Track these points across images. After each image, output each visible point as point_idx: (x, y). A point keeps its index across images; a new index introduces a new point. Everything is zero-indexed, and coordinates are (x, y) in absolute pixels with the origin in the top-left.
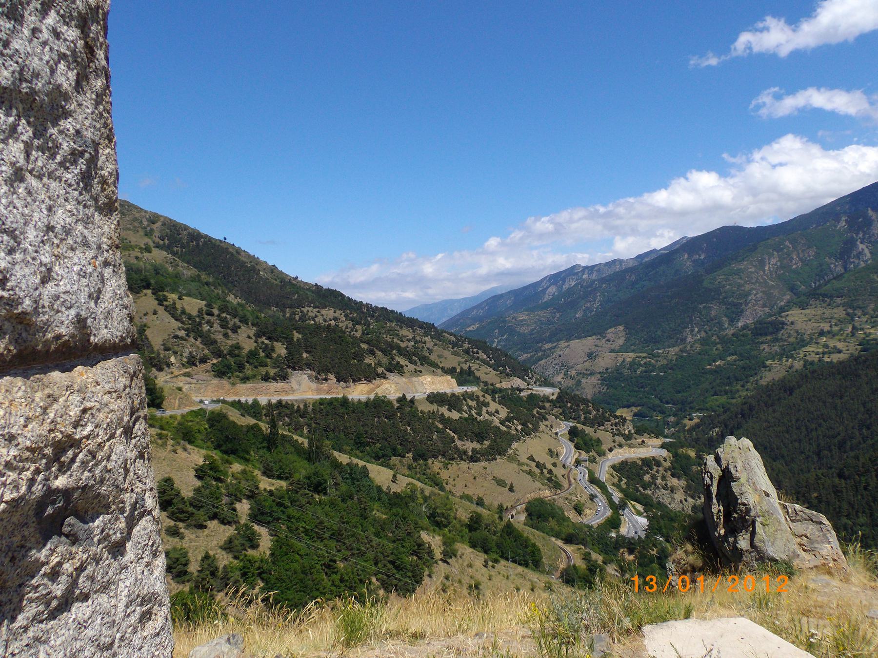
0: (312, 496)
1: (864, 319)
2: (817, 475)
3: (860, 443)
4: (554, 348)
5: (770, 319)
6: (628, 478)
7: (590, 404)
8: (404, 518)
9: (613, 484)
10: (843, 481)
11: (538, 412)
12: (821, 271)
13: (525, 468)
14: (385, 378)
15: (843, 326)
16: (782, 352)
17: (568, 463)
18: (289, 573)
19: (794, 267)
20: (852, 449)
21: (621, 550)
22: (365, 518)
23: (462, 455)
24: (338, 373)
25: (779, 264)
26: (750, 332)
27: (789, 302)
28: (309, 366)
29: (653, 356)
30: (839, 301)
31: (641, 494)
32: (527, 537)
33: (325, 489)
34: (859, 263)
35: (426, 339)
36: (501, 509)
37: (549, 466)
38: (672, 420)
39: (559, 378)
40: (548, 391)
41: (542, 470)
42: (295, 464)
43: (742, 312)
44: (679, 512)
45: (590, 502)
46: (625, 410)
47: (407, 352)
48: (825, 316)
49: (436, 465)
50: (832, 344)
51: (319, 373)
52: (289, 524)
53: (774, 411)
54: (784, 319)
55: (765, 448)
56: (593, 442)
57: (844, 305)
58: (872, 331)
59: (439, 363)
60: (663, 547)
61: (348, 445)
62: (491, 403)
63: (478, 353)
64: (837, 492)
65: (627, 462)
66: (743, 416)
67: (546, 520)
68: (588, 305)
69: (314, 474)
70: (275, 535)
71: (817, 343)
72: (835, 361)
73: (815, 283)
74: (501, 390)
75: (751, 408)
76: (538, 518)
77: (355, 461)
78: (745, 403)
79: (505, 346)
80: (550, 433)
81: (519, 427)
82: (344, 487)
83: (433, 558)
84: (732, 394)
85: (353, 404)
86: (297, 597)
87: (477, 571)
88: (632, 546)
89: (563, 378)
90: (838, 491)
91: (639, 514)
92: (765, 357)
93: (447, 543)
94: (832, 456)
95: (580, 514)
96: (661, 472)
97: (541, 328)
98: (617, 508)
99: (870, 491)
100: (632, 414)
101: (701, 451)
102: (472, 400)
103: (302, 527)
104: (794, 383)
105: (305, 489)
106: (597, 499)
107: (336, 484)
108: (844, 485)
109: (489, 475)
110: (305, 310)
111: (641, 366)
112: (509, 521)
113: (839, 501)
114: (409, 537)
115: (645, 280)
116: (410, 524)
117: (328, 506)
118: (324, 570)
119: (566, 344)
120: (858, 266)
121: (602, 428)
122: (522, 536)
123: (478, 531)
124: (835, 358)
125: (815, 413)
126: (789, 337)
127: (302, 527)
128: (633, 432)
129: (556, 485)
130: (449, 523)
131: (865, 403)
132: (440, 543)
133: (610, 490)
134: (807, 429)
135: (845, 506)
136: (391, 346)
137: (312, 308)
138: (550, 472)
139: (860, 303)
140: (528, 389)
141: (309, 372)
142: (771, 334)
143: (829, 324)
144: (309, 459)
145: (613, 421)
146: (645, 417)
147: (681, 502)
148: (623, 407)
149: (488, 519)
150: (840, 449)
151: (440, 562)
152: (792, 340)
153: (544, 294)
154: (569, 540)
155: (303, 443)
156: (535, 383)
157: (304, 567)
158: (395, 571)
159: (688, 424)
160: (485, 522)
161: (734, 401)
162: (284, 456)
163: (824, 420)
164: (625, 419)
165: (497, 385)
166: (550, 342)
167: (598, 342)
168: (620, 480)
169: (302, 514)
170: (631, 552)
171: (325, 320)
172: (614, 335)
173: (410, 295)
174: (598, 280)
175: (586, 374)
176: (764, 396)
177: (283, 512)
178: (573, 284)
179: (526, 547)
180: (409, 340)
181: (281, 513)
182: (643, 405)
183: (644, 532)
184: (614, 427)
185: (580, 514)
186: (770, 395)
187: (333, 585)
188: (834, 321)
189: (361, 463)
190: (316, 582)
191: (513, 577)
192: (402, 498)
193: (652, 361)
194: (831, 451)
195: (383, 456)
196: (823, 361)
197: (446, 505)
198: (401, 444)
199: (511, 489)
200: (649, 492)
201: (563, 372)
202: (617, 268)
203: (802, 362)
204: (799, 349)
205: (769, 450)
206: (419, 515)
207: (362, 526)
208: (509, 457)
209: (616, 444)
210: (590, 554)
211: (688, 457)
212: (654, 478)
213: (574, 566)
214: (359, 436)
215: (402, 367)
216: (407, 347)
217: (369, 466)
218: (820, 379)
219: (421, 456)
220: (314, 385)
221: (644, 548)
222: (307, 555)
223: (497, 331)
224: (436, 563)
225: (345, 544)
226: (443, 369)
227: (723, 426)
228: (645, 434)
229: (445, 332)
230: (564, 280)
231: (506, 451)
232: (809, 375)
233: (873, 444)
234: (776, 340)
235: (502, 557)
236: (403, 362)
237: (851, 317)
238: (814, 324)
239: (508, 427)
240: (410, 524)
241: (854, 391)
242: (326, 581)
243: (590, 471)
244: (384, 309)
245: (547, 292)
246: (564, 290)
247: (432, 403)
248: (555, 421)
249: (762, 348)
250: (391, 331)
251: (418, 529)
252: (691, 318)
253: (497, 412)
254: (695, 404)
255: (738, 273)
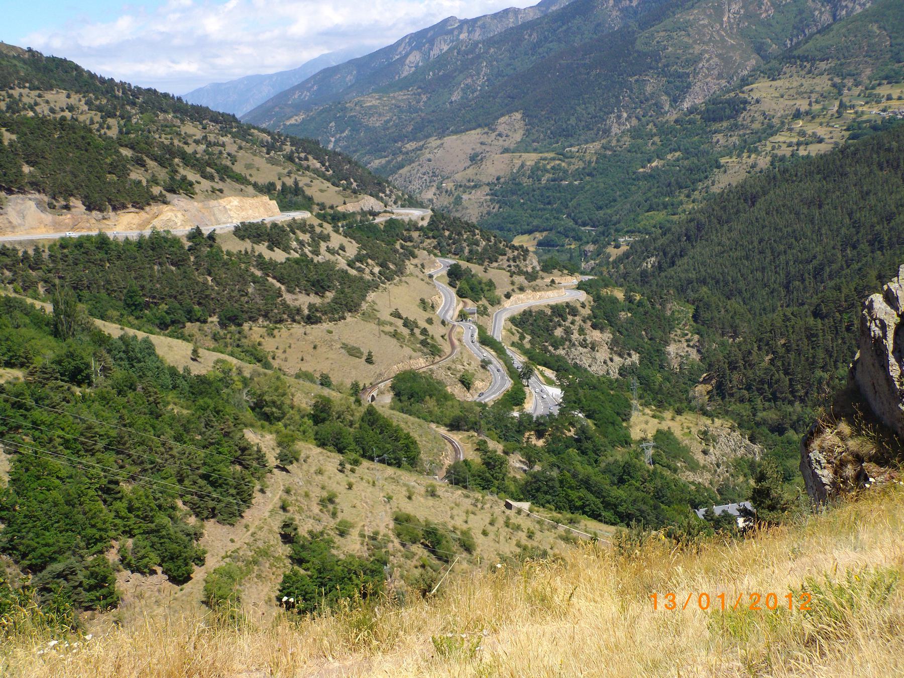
0: (69, 389)
1: (856, 91)
2: (785, 315)
3: (842, 268)
4: (420, 149)
5: (727, 96)
6: (532, 333)
7: (477, 231)
8: (218, 412)
9: (513, 344)
10: (819, 321)
11: (402, 247)
12: (801, 21)
13: (388, 328)
14: (165, 203)
15: (827, 102)
16: (743, 144)
17: (448, 318)
18: (45, 506)
19: (764, 15)
20: (831, 277)
21: (527, 434)
22: (158, 416)
23: (294, 314)
24: (86, 197)
25: (742, 12)
26: (699, 117)
27: (753, 70)
28: (37, 186)
29: (564, 156)
30: (823, 65)
31: (551, 356)
32: (398, 426)
33: (88, 377)
34: (853, 8)
35: (224, 139)
36: (356, 390)
37: (423, 324)
38: (591, 249)
39: (429, 194)
40: (414, 214)
41: (412, 330)
42: (33, 342)
43: (689, 86)
44: (603, 376)
45: (482, 370)
46: (526, 237)
47: (197, 160)
48: (802, 89)
49: (255, 331)
50: (810, 129)
51: (54, 198)
52: (37, 433)
53: (730, 230)
54: (746, 96)
55: (717, 282)
56: (483, 286)
57: (829, 71)
58: (865, 109)
59: (248, 177)
60: (582, 426)
61: (115, 309)
62: (334, 235)
63: (307, 159)
64: (811, 335)
65: (530, 311)
66: (689, 238)
67: (421, 400)
68: (469, 81)
69: (68, 356)
70: (15, 452)
71: (790, 130)
72: (813, 154)
73: (791, 40)
74: (344, 216)
75: (699, 227)
76: (409, 399)
77: (131, 332)
78: (691, 220)
79: (346, 147)
80: (421, 275)
81: (377, 270)
82: (119, 374)
83: (265, 466)
84: (673, 208)
85: (117, 245)
86: (62, 540)
87: (330, 478)
88: (541, 428)
89: (435, 194)
90: (813, 335)
91: (550, 382)
92: (719, 153)
93: (284, 443)
94: (805, 288)
95: (468, 389)
96: (577, 324)
97: (400, 118)
98: (520, 376)
99: (853, 332)
100: (535, 242)
101: (631, 291)
102: (304, 232)
103: (59, 437)
104: (758, 189)
105: (56, 379)
106: (491, 366)
107: (104, 369)
108: (820, 326)
109: (335, 341)
110: (16, 93)
111: (547, 171)
112: (371, 406)
113: (813, 348)
114: (226, 439)
115: (552, 42)
116: (228, 420)
117: (97, 403)
118: (100, 496)
119: (439, 142)
120: (852, 12)
121: (495, 264)
122: (390, 425)
123: (327, 422)
124: (814, 150)
125: (785, 230)
126: (752, 122)
127: (59, 437)
128: (538, 268)
129: (432, 350)
130: (284, 414)
131: (852, 213)
132: (273, 443)
133: (508, 352)
134: (773, 252)
135: (821, 354)
136: (172, 152)
137: (27, 90)
138: (424, 332)
139: (852, 68)
140: (385, 212)
141: (37, 196)
142: (729, 118)
143: (807, 101)
144: (56, 333)
145: (510, 254)
146: (553, 246)
147: (605, 362)
148: (523, 234)
149: (341, 405)
150: (815, 278)
151: (276, 471)
152: (756, 126)
153: (403, 64)
154: (455, 426)
155: (42, 308)
156: (395, 203)
157: (69, 495)
158: (210, 489)
159: (614, 253)
160: (337, 409)
161: (676, 217)
162: (14, 332)
163: (796, 240)
164: (527, 250)
165: (339, 209)
166: (415, 139)
167: (484, 138)
168: (522, 338)
169: (56, 418)
170: (540, 435)
171: (52, 111)
172: (507, 127)
173: (189, 67)
174: (483, 42)
175: (469, 187)
176: (716, 208)
177: (25, 417)
178: (445, 48)
179: (397, 439)
180: (197, 142)
181: (21, 418)
182: (551, 230)
183: (558, 407)
184: (512, 263)
185: (468, 389)
186: (725, 206)
187: (117, 516)
188: (814, 97)
189: (141, 335)
190: (90, 515)
191: (381, 482)
192: (210, 383)
193: (563, 164)
194: (803, 280)
195: (173, 322)
196: (798, 155)
197: (276, 389)
198: (199, 304)
199: (369, 361)
200: (561, 352)
201: (435, 184)
202: (511, 22)
203: (769, 158)
204: (766, 139)
205: (722, 284)
206: (238, 405)
207: (154, 428)
208: (363, 314)
209: (515, 287)
210: (485, 442)
211: (614, 301)
212: (568, 331)
213: (465, 461)
214: (131, 294)
215: (191, 184)
216: (196, 152)
217: (153, 338)
218: (793, 182)
219: (231, 319)
220: (48, 217)
221: (557, 428)
222: (71, 477)
223: (333, 124)
224: (271, 472)
225: (129, 456)
226: (255, 186)
227: (661, 254)
228: (555, 271)
229: (254, 128)
230: (432, 42)
231: (359, 305)
232: (779, 176)
233: (860, 269)
234: (735, 127)
235: (363, 456)
236: (192, 176)
237: (838, 89)
238: (787, 102)
239: (360, 270)
240: (228, 420)
241: (838, 197)
242: (106, 513)
243: (480, 328)
244: (151, 92)
245: (407, 62)
246: (431, 59)
247: (242, 238)
248: (428, 257)
249: (715, 140)
250: (166, 127)
251: (240, 426)
252: (617, 97)
253: (342, 248)
254: (622, 224)
255: (683, 27)
